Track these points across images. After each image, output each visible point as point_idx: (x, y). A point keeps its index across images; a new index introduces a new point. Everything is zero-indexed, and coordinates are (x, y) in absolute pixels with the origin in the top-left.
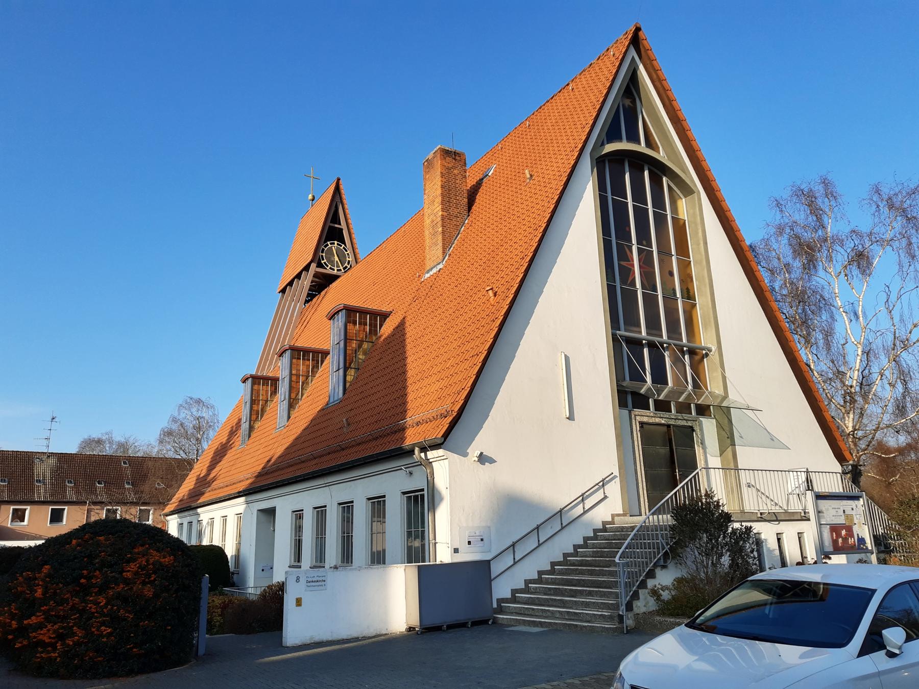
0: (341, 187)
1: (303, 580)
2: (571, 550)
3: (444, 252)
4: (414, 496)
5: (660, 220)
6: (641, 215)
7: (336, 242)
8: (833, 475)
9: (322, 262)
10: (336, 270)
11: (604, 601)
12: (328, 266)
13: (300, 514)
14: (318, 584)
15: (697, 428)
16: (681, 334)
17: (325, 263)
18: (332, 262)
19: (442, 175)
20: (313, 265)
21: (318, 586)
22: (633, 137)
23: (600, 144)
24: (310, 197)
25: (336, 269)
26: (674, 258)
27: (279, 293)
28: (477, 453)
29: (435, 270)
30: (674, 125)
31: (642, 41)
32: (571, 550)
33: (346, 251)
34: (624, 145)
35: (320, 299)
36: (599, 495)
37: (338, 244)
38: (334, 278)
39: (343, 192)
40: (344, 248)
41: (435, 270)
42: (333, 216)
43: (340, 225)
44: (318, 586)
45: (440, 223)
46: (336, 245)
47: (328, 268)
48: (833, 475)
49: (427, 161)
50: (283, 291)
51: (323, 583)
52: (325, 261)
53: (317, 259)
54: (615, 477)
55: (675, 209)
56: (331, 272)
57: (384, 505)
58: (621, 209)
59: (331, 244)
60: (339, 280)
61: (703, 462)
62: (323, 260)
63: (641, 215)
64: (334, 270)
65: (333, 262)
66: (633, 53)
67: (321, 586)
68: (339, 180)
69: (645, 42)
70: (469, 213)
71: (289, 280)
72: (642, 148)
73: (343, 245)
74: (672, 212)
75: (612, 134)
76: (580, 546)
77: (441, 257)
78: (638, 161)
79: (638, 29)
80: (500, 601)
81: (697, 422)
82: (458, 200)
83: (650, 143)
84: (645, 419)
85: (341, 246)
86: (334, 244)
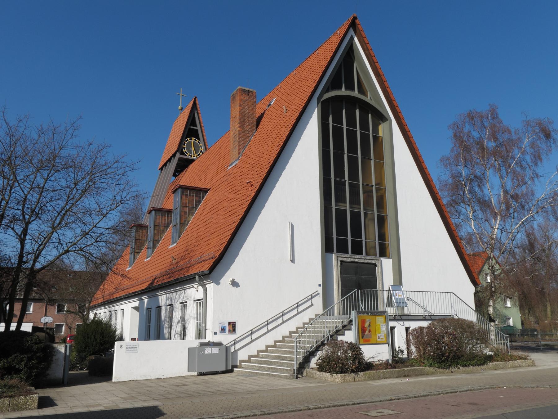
0: (197, 102)
1: (124, 347)
2: (288, 334)
3: (239, 153)
4: (199, 302)
5: (365, 138)
6: (352, 135)
7: (193, 138)
8: (450, 295)
9: (184, 151)
10: (193, 156)
11: (291, 362)
12: (187, 154)
13: (185, 305)
14: (133, 349)
15: (378, 264)
16: (373, 208)
17: (186, 152)
18: (190, 152)
19: (240, 105)
20: (178, 155)
21: (133, 350)
22: (350, 87)
23: (327, 90)
24: (180, 107)
25: (193, 155)
26: (372, 162)
27: (159, 170)
28: (231, 279)
29: (234, 165)
30: (377, 78)
31: (358, 25)
32: (288, 334)
33: (200, 144)
34: (343, 92)
35: (182, 176)
36: (309, 303)
37: (194, 140)
38: (191, 161)
39: (198, 106)
40: (198, 142)
41: (234, 165)
42: (192, 121)
43: (197, 127)
44: (133, 350)
45: (238, 135)
46: (193, 140)
47: (187, 155)
48: (450, 295)
49: (232, 95)
50: (161, 169)
51: (136, 349)
52: (186, 150)
53: (180, 150)
54: (318, 294)
55: (376, 130)
56: (189, 157)
57: (151, 312)
58: (338, 132)
59: (190, 139)
60: (194, 163)
61: (380, 285)
62: (185, 150)
63: (352, 135)
64: (191, 156)
65: (191, 151)
66: (352, 32)
67: (134, 350)
68: (196, 98)
69: (359, 26)
70: (257, 128)
71: (165, 162)
72: (356, 93)
73: (198, 140)
74: (373, 132)
75: (334, 84)
76: (293, 332)
77: (237, 157)
78: (352, 102)
79: (355, 18)
80: (242, 361)
81: (379, 261)
82: (250, 120)
83: (361, 90)
84: (344, 259)
85: (196, 140)
86: (192, 139)
